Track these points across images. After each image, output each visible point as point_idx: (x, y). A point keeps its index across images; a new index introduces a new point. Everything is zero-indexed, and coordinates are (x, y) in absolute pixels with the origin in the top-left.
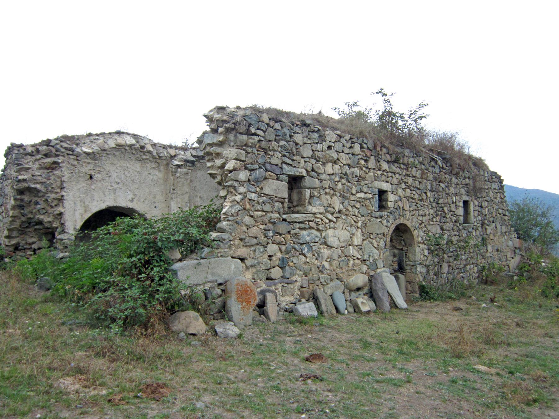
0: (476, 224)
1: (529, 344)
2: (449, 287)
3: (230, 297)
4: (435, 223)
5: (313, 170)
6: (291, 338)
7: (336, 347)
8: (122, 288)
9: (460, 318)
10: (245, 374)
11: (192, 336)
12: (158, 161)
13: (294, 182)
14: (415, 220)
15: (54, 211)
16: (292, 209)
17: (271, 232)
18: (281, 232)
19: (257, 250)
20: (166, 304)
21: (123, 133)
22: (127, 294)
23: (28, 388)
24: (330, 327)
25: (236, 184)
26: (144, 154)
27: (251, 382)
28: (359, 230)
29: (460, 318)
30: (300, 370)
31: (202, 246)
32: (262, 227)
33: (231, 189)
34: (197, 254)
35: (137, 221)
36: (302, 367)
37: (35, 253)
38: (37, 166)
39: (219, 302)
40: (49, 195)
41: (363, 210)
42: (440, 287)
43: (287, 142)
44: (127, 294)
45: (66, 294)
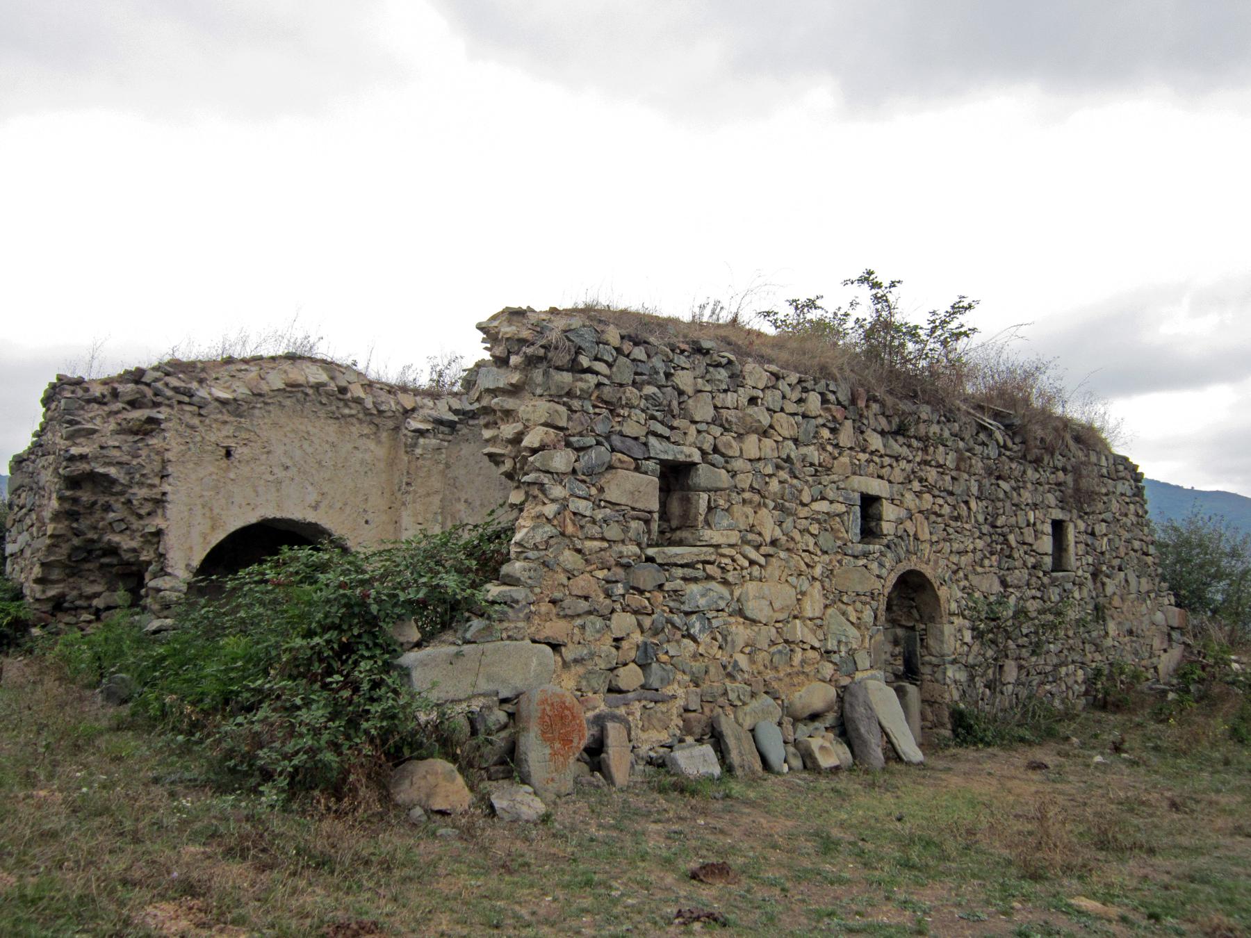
0: (1080, 573)
1: (1197, 851)
2: (1018, 716)
3: (525, 729)
4: (987, 569)
5: (716, 450)
6: (659, 827)
7: (759, 849)
8: (288, 704)
9: (1040, 787)
10: (553, 905)
11: (438, 817)
12: (377, 420)
13: (675, 476)
14: (942, 563)
15: (144, 526)
16: (668, 535)
17: (620, 585)
18: (642, 587)
19: (589, 625)
20: (384, 742)
21: (301, 358)
22: (299, 719)
23: (78, 924)
24: (748, 803)
25: (545, 479)
26: (346, 405)
27: (566, 925)
28: (817, 584)
29: (1040, 787)
30: (677, 900)
31: (467, 614)
32: (601, 574)
33: (535, 491)
34: (456, 631)
35: (327, 557)
36: (682, 893)
37: (98, 619)
38: (112, 426)
39: (500, 740)
40: (135, 490)
41: (826, 540)
42: (1000, 715)
43: (659, 387)
44: (299, 719)
45: (164, 713)
